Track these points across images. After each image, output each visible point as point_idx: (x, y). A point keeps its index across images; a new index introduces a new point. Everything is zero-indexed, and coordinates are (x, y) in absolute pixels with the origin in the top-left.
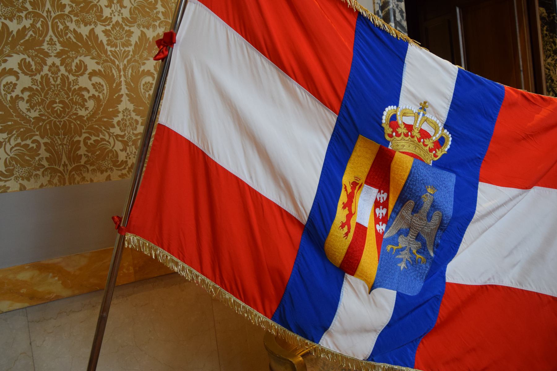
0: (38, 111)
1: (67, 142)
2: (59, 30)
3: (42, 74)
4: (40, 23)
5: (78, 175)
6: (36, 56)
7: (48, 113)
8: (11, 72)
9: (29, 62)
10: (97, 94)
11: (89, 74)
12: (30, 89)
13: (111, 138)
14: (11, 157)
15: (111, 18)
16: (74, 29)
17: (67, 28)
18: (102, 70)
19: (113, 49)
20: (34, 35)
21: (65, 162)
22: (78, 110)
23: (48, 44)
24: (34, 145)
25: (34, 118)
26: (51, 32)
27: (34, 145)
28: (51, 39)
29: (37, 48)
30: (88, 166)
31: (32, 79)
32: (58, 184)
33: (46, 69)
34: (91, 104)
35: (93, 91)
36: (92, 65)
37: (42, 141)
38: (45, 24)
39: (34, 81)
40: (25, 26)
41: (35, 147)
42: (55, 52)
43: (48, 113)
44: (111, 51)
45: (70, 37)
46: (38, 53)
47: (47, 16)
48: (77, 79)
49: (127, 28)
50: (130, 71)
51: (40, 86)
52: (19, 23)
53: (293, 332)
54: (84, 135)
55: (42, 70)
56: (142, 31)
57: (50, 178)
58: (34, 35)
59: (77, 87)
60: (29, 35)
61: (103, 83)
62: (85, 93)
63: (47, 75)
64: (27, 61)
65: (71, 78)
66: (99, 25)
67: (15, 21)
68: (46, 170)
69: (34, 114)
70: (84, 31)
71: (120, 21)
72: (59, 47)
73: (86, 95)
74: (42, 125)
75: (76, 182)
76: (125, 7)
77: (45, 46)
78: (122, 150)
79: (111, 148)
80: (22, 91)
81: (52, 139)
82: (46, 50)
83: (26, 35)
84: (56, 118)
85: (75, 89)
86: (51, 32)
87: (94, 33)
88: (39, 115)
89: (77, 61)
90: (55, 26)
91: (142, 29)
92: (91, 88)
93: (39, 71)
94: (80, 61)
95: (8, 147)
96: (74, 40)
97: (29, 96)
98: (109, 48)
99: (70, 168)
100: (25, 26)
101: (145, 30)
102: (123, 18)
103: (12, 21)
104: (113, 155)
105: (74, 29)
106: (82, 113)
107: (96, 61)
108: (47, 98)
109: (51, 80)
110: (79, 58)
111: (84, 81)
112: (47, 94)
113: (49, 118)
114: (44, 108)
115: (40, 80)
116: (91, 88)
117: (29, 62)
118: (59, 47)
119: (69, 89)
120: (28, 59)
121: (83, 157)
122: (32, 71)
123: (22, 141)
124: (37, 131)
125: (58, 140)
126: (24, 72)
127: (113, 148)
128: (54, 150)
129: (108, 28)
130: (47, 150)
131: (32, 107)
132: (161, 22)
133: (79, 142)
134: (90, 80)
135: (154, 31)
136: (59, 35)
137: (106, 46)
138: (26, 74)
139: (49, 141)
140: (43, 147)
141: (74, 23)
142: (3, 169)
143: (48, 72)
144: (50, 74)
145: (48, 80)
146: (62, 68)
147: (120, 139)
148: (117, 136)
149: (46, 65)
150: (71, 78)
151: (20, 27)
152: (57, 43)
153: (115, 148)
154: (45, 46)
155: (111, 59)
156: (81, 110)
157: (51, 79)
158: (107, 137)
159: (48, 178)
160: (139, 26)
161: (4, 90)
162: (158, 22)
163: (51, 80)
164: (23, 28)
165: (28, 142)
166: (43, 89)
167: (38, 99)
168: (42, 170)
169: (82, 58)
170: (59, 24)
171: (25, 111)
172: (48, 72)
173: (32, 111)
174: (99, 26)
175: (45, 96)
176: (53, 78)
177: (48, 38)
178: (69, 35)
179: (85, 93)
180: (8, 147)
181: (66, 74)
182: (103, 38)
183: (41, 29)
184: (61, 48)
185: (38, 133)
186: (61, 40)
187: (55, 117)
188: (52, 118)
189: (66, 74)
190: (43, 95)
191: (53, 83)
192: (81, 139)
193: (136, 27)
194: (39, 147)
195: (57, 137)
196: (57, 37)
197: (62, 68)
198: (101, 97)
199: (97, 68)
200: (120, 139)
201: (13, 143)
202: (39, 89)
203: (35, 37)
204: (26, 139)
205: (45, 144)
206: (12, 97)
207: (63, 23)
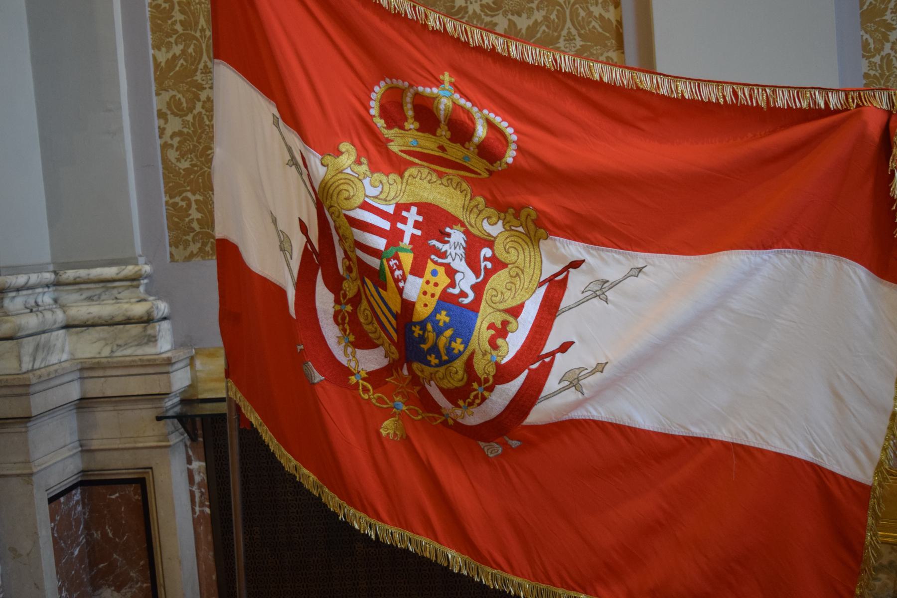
2: (580, 18)
3: (195, 112)
4: (192, 46)
6: (876, 30)
7: (201, 162)
9: (179, 99)
12: (179, 133)
15: (467, 7)
16: (600, 14)
17: (590, 14)
20: (547, 30)
23: (202, 73)
24: (184, 204)
25: (184, 170)
26: (569, 24)
27: (184, 204)
28: (569, 33)
31: (183, 121)
33: (199, 105)
37: (193, 198)
38: (561, 16)
39: (185, 124)
40: (536, 20)
42: (573, 49)
43: (201, 162)
45: (594, 27)
47: (201, 37)
49: (487, 19)
52: (528, 18)
53: (356, 508)
56: (509, 20)
60: (541, 31)
63: (889, 54)
64: (177, 98)
67: (164, 49)
69: (185, 164)
71: (478, 11)
72: (579, 43)
77: (199, 77)
80: (172, 137)
81: (205, 196)
82: (200, 81)
83: (538, 31)
86: (569, 24)
90: (574, 14)
91: (510, 16)
93: (878, 51)
96: (600, 30)
97: (179, 142)
100: (536, 20)
101: (515, 18)
102: (482, 6)
103: (520, 16)
105: (600, 14)
108: (199, 143)
110: (606, 55)
112: (200, 137)
114: (196, 156)
115: (192, 120)
117: (179, 99)
118: (579, 43)
120: (179, 96)
122: (182, 110)
126: (173, 113)
130: (198, 210)
131: (182, 156)
132: (179, 37)
135: (167, 52)
136: (579, 23)
138: (176, 115)
139: (201, 198)
140: (194, 206)
141: (600, 5)
144: (204, 112)
145: (201, 120)
149: (199, 100)
151: (531, 22)
152: (577, 37)
154: (199, 77)
159: (199, 245)
160: (505, 14)
162: (175, 37)
164: (534, 24)
165: (177, 199)
166: (882, 75)
168: (192, 234)
170: (580, 10)
171: (174, 161)
172: (890, 51)
173: (183, 161)
175: (197, 142)
176: (208, 117)
177: (564, 33)
178: (593, 23)
183: (556, 20)
185: (188, 188)
186: (582, 32)
191: (207, 123)
193: (501, 15)
194: (189, 206)
196: (576, 29)
204: (175, 197)
205: (196, 201)
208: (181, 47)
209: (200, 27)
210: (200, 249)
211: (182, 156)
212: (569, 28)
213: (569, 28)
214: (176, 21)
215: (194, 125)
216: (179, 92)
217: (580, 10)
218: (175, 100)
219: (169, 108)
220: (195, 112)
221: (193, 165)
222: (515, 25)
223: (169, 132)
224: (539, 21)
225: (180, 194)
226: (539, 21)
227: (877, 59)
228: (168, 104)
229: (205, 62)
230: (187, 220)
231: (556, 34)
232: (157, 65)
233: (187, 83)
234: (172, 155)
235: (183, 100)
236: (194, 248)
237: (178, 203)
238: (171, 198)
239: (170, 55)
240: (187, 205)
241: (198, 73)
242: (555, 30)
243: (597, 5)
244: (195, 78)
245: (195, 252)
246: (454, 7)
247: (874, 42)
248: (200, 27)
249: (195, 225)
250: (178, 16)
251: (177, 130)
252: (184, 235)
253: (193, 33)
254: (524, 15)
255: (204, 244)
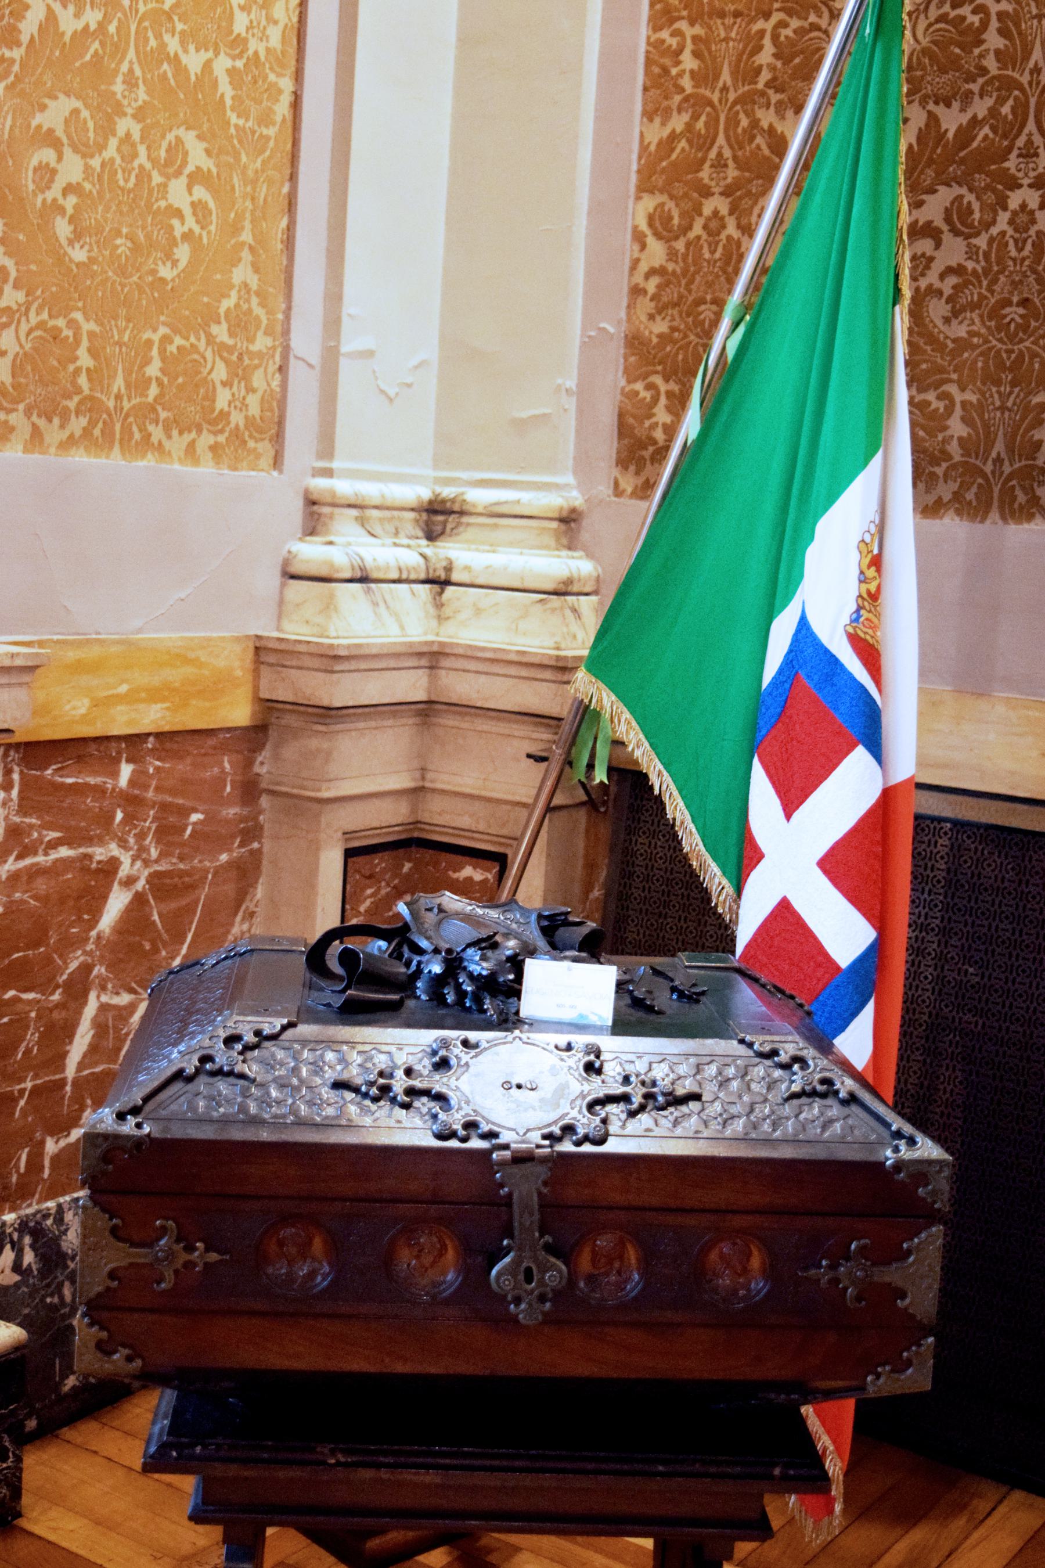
0: (966, 322)
1: (1014, 404)
2: (740, 130)
3: (994, 231)
4: (1011, 102)
5: (1023, 488)
6: (988, 187)
7: (989, 328)
8: (49, 139)
9: (969, 203)
10: (197, 229)
11: (189, 176)
12: (660, 271)
13: (210, 349)
14: (25, 354)
16: (771, 126)
17: (755, 124)
18: (214, 170)
19: (241, 122)
20: (991, 135)
21: (999, 453)
22: (160, 263)
25: (954, 341)
28: (720, 154)
29: (993, 167)
30: (159, 408)
31: (969, 245)
32: (974, 504)
33: (1003, 217)
34: (183, 253)
35: (191, 222)
36: (197, 156)
37: (958, 397)
38: (713, 123)
41: (941, 410)
42: (1032, 174)
44: (236, 126)
46: (993, 181)
47: (1030, 83)
48: (165, 185)
50: (264, 190)
51: (983, 263)
54: (163, 330)
55: (994, 222)
56: (929, 112)
57: (960, 487)
58: (100, 52)
59: (163, 204)
60: (980, 137)
61: (212, 204)
62: (175, 222)
65: (157, 179)
66: (222, 55)
68: (954, 467)
69: (79, 255)
70: (194, 61)
73: (179, 230)
74: (967, 359)
75: (1016, 506)
76: (276, 22)
77: (118, 87)
78: (224, 384)
79: (205, 371)
81: (983, 394)
84: (1004, 343)
85: (159, 208)
87: (211, 72)
88: (968, 332)
89: (170, 137)
91: (931, 106)
92: (187, 211)
94: (177, 138)
95: (24, 327)
98: (234, 119)
99: (1007, 469)
101: (940, 110)
103: (948, 105)
104: (207, 392)
106: (166, 272)
107: (204, 145)
108: (992, 292)
109: (120, 176)
111: (178, 194)
113: (986, 341)
115: (984, 246)
116: (187, 211)
118: (142, 95)
119: (149, 205)
121: (154, 385)
122: (971, 226)
123: (50, 316)
124: (955, 371)
125: (996, 396)
127: (209, 373)
128: (982, 419)
129: (239, 64)
132: (686, 99)
133: (149, 343)
134: (191, 194)
135: (963, 110)
137: (229, 113)
138: (956, 233)
140: (958, 411)
141: (772, 108)
142: (8, 380)
143: (115, 155)
144: (1010, 232)
146: (142, 150)
147: (225, 354)
148: (223, 346)
150: (157, 179)
151: (964, 119)
152: (730, 163)
153: (213, 375)
154: (1012, 163)
155: (233, 146)
156: (164, 263)
157: (120, 171)
158: (202, 345)
159: (954, 486)
161: (34, 181)
163: (120, 176)
167: (972, 294)
169: (181, 132)
170: (742, 116)
174: (222, 56)
179: (175, 222)
180: (24, 327)
181: (148, 166)
182: (225, 88)
183: (1010, 117)
184: (146, 98)
185: (955, 376)
187: (1000, 340)
188: (994, 342)
189: (148, 166)
190: (985, 283)
192: (156, 338)
194: (949, 410)
195: (994, 389)
197: (142, 150)
198: (205, 241)
199: (207, 164)
200: (225, 354)
201: (34, 319)
202: (980, 270)
203: (993, 140)
205: (964, 404)
206: (44, 200)
207: (158, 36)
208: (989, 102)
209: (1031, 64)
210: (955, 493)
211: (956, 313)
212: (1030, 134)
213: (1030, 134)
214: (987, 51)
215: (987, 255)
216: (971, 190)
217: (742, 116)
218: (961, 203)
219: (948, 220)
220: (994, 231)
221: (972, 334)
222: (55, 18)
223: (644, 267)
224: (980, 117)
225: (937, 385)
226: (980, 117)
227: (680, 245)
228: (948, 212)
229: (721, 147)
230: (647, 423)
231: (1006, 143)
232: (644, 148)
233: (686, 183)
234: (937, 309)
235: (976, 206)
236: (77, 424)
237: (929, 404)
238: (629, 382)
239: (80, 25)
240: (946, 407)
241: (1013, 156)
242: (1005, 136)
243: (768, 108)
244: (1006, 165)
245: (946, 499)
246: (232, 32)
247: (981, 210)
248: (720, 84)
249: (954, 448)
250: (993, 40)
251: (657, 265)
252: (931, 464)
253: (1016, 75)
254: (956, 105)
255: (964, 486)
